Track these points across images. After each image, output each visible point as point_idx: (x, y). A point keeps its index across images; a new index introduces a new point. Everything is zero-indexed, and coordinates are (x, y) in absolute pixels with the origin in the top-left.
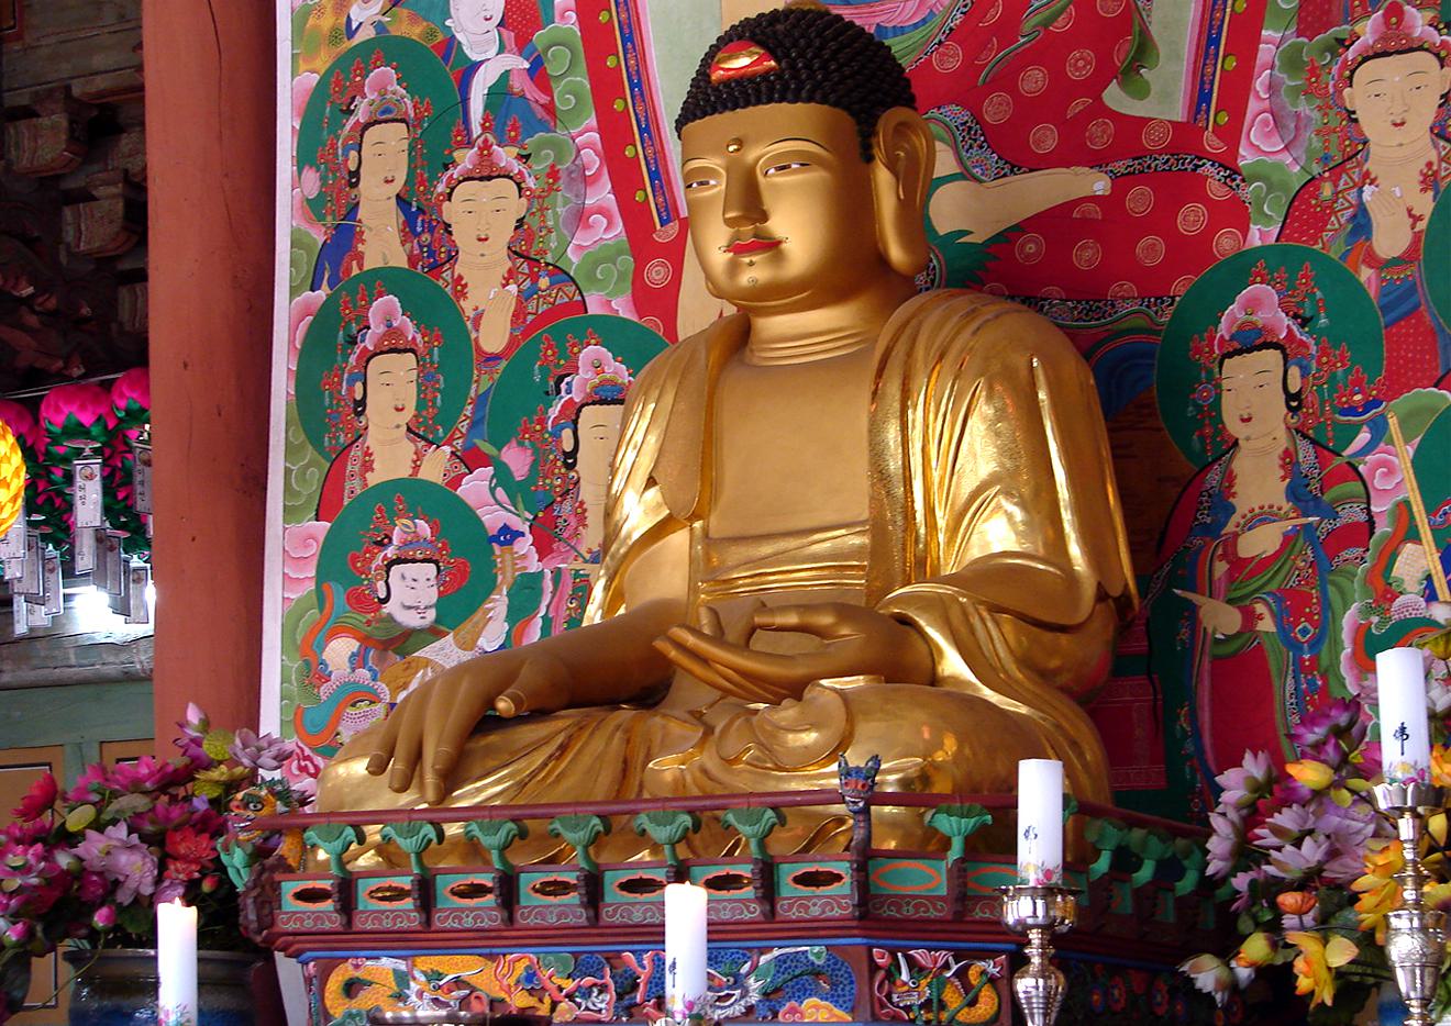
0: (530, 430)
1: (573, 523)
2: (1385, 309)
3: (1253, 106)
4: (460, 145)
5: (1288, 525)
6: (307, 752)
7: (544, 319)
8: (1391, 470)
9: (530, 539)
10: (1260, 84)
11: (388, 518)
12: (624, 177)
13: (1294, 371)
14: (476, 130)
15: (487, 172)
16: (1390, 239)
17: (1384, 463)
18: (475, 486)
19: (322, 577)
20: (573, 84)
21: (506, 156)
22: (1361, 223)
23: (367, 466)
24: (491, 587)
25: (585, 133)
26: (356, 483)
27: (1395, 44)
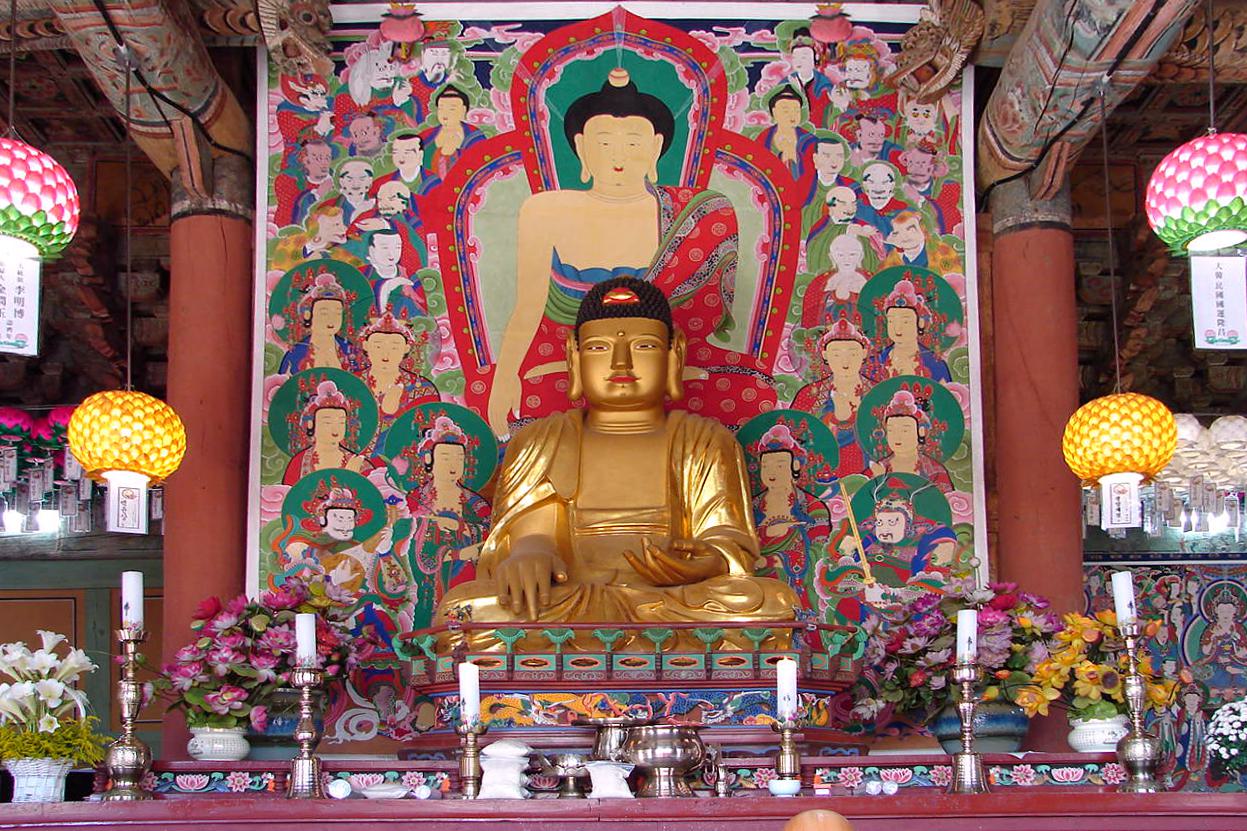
0: (408, 452)
1: (429, 497)
2: (839, 441)
3: (780, 352)
4: (373, 316)
5: (792, 525)
8: (841, 506)
9: (406, 502)
10: (784, 343)
12: (462, 343)
13: (797, 463)
15: (388, 330)
16: (843, 412)
17: (838, 503)
18: (377, 476)
20: (436, 296)
21: (399, 324)
23: (315, 460)
24: (385, 524)
25: (443, 319)
26: (308, 468)
27: (843, 336)
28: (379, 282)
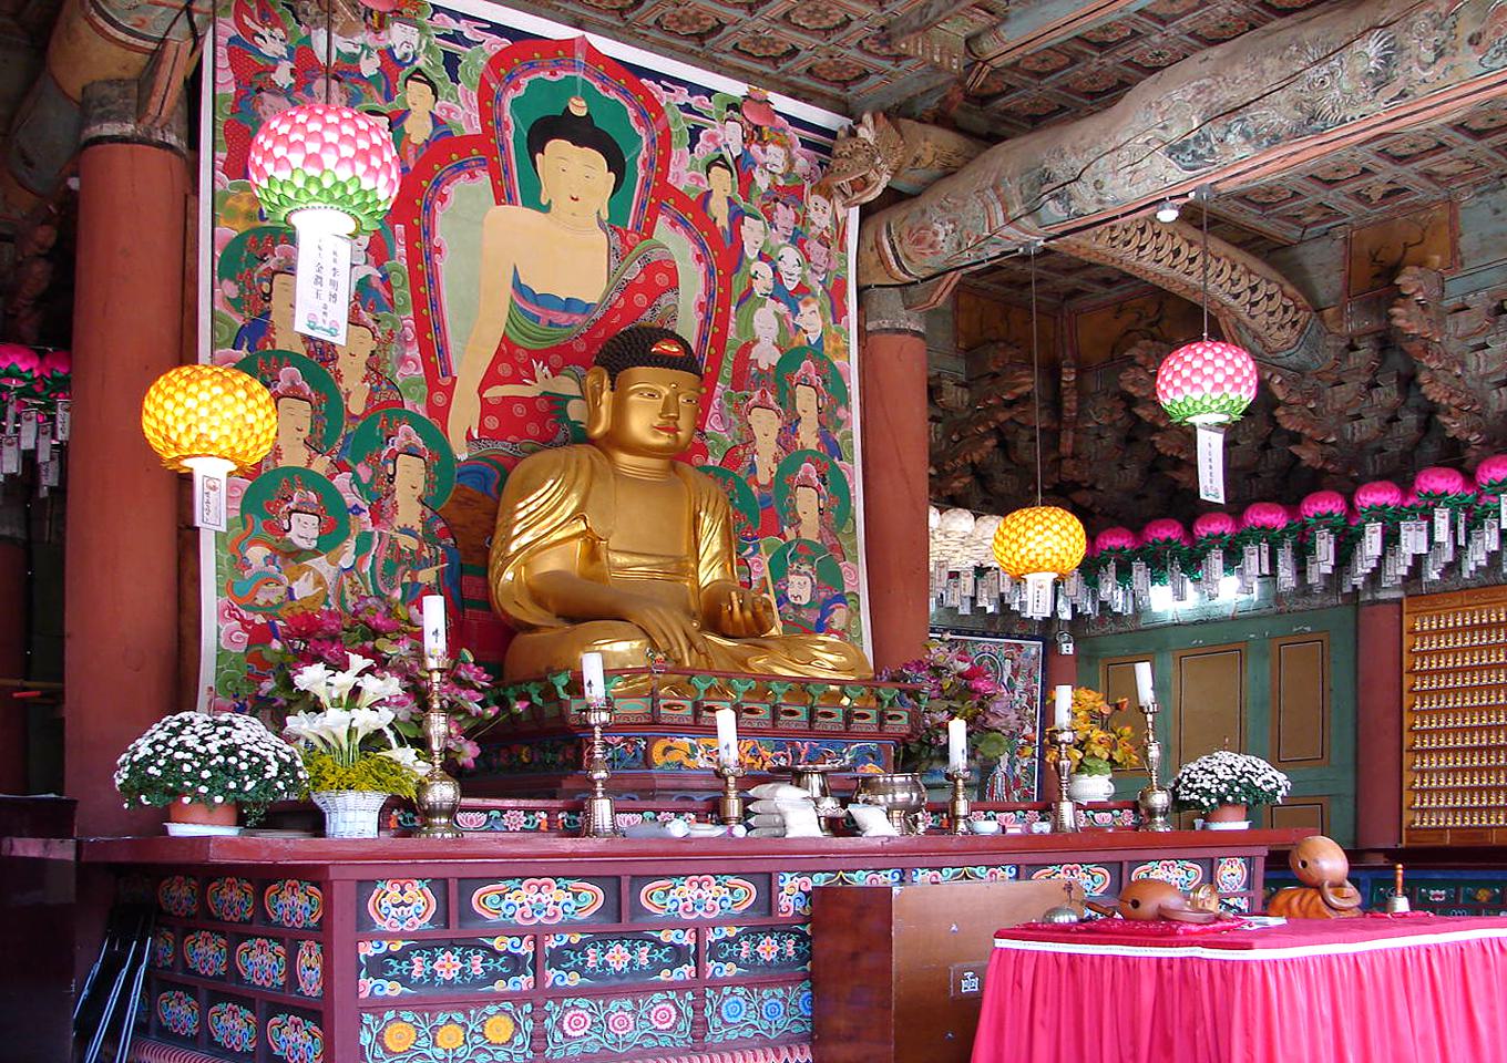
0: (372, 460)
1: (391, 510)
3: (712, 410)
7: (381, 406)
8: (760, 565)
11: (291, 486)
12: (426, 349)
16: (763, 477)
18: (342, 481)
20: (403, 294)
22: (753, 468)
24: (348, 536)
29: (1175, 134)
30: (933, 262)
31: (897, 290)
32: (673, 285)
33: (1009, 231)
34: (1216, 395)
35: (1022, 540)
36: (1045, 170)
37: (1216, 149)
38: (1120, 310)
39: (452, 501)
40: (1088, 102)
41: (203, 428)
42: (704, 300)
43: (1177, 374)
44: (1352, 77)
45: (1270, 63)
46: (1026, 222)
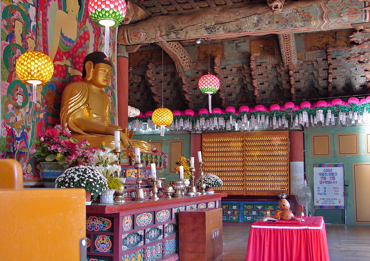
6: (5, 123)
14: (31, 31)
19: (8, 92)
24: (27, 103)
28: (31, 21)
29: (208, 25)
30: (137, 42)
31: (124, 46)
32: (89, 39)
33: (160, 38)
34: (214, 88)
35: (162, 116)
36: (173, 26)
37: (217, 31)
38: (141, 54)
39: (47, 94)
40: (161, 6)
41: (42, 72)
42: (94, 44)
43: (202, 82)
44: (250, 23)
45: (232, 15)
46: (165, 37)
